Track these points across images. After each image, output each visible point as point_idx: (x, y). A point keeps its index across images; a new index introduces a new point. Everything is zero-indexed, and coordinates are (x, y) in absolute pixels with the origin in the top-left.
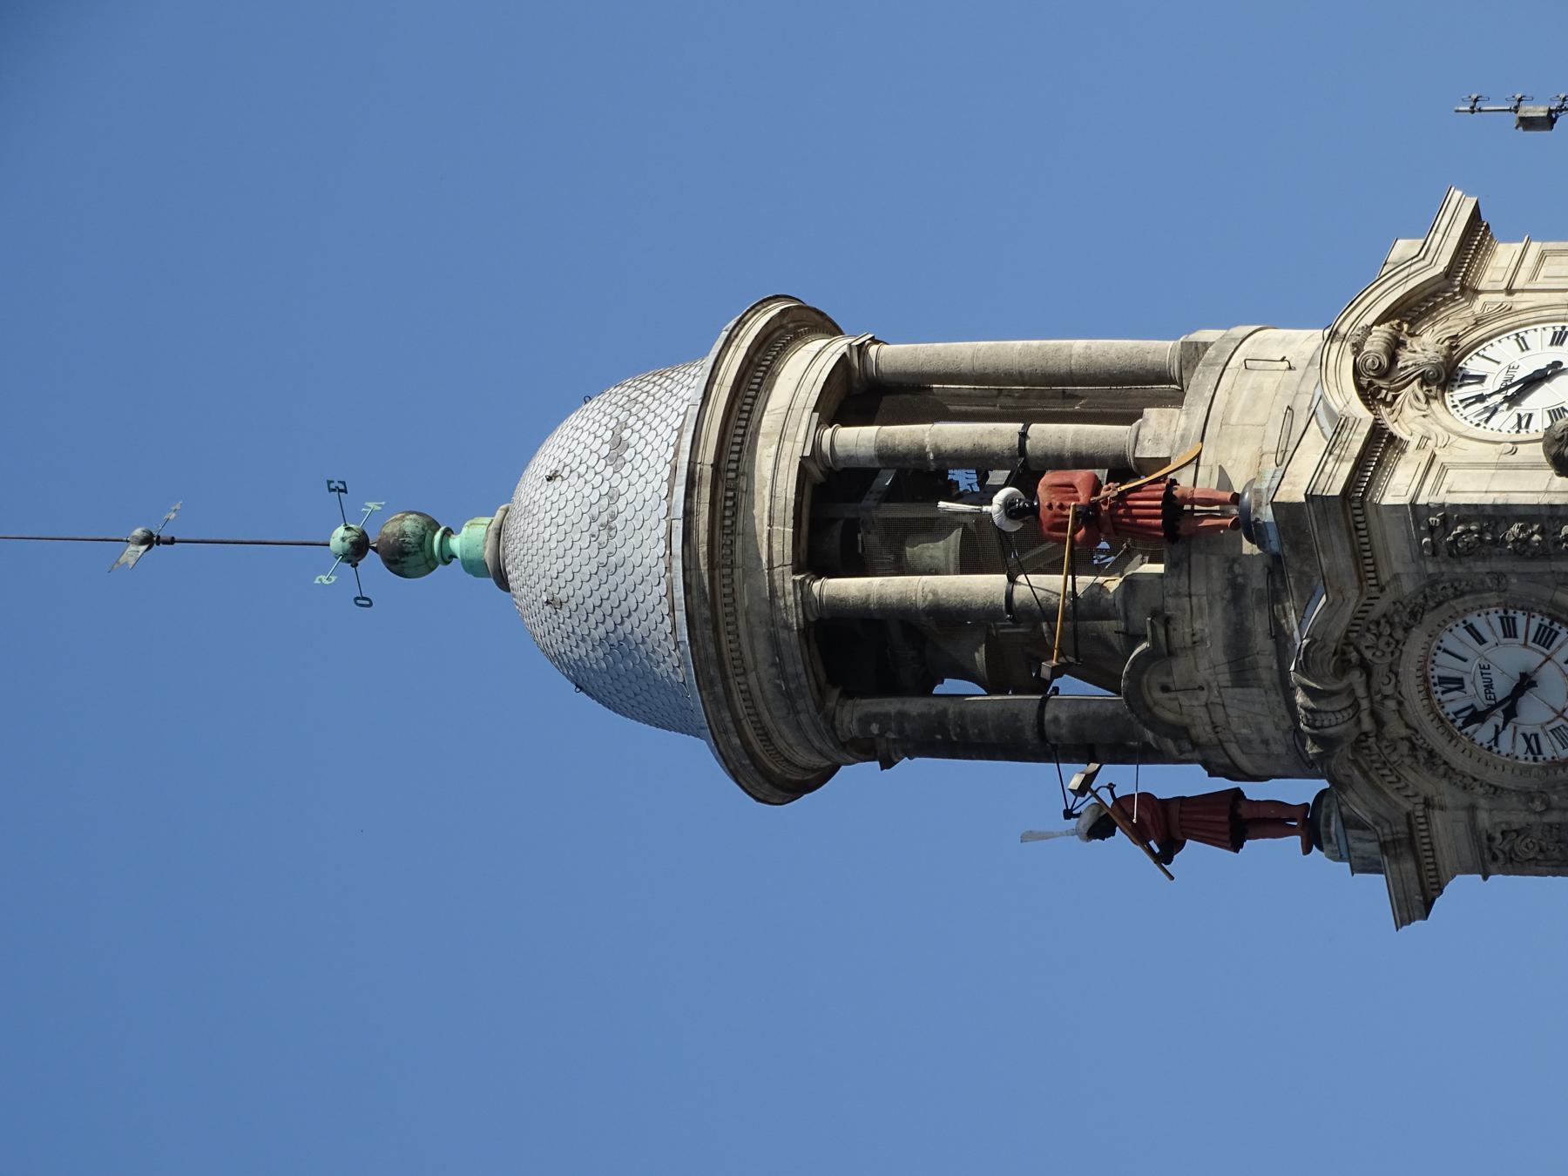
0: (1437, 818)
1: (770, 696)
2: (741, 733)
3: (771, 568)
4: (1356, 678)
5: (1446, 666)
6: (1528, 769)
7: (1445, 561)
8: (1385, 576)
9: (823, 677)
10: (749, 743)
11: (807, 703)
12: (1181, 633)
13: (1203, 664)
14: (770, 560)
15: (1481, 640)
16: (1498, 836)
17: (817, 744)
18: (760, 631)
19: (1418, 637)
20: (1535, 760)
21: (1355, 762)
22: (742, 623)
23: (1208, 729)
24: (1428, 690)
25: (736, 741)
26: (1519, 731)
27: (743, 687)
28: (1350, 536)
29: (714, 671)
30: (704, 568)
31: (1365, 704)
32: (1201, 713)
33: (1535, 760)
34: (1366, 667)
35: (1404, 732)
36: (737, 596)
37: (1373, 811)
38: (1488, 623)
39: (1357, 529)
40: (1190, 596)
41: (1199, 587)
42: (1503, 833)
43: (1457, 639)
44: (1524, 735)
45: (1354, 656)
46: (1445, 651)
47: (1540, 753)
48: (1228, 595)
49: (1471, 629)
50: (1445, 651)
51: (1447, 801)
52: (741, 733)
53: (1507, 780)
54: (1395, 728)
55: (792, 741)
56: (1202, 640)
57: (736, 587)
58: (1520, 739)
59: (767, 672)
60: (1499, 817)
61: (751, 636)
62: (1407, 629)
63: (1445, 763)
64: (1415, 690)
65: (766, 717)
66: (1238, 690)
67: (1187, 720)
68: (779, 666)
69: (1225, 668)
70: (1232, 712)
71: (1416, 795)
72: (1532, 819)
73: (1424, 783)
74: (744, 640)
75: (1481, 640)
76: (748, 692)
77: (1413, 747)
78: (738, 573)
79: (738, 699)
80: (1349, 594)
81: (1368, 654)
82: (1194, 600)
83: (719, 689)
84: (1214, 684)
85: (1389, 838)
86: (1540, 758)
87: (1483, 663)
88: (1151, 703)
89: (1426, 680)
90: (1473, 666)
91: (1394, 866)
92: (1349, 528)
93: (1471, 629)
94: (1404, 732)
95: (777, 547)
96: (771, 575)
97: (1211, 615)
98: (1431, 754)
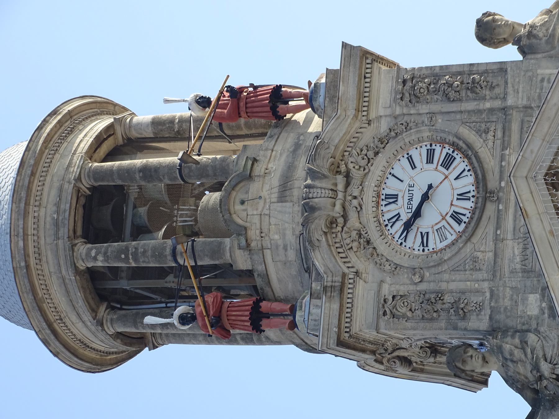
0: (360, 284)
1: (48, 227)
2: (25, 240)
3: (74, 154)
4: (341, 180)
5: (392, 186)
6: (418, 257)
7: (407, 106)
8: (372, 115)
9: (79, 232)
10: (29, 256)
11: (64, 232)
12: (259, 169)
13: (267, 187)
14: (76, 150)
15: (413, 167)
16: (391, 299)
17: (64, 272)
18: (56, 185)
19: (380, 161)
20: (423, 250)
21: (325, 233)
22: (48, 179)
23: (258, 232)
24: (378, 203)
25: (21, 244)
26: (420, 230)
27: (36, 214)
28: (360, 80)
29: (23, 194)
30: (41, 142)
31: (340, 195)
32: (256, 220)
33: (423, 250)
34: (348, 176)
35: (357, 225)
36: (52, 165)
37: (326, 266)
38: (419, 154)
39: (365, 78)
40: (272, 151)
41: (278, 148)
42: (394, 297)
43: (401, 167)
44: (421, 233)
45: (343, 168)
46: (393, 175)
47: (427, 246)
48: (291, 150)
49: (410, 159)
50: (393, 175)
51: (370, 278)
52: (25, 240)
53: (405, 262)
54: (353, 221)
55: (52, 270)
56: (270, 173)
57: (54, 161)
58: (419, 235)
59: (51, 208)
60: (394, 289)
61: (50, 188)
62: (376, 154)
63: (374, 248)
64: (371, 199)
65: (42, 242)
66: (280, 204)
67: (247, 225)
68: (58, 205)
69: (276, 190)
70: (273, 221)
71: (352, 267)
72: (412, 288)
73: (359, 261)
74: (46, 188)
75: (413, 167)
76: (37, 218)
77: (360, 235)
78: (57, 156)
79: (31, 220)
80: (349, 113)
81: (351, 166)
82: (274, 152)
83: (22, 205)
84: (268, 201)
85: (329, 284)
86: (426, 249)
87: (411, 183)
88: (232, 212)
89: (379, 196)
90: (404, 186)
91: (327, 305)
92: (360, 75)
93: (410, 159)
94: (357, 225)
95: (82, 145)
96: (73, 156)
97: (279, 160)
98: (368, 242)
